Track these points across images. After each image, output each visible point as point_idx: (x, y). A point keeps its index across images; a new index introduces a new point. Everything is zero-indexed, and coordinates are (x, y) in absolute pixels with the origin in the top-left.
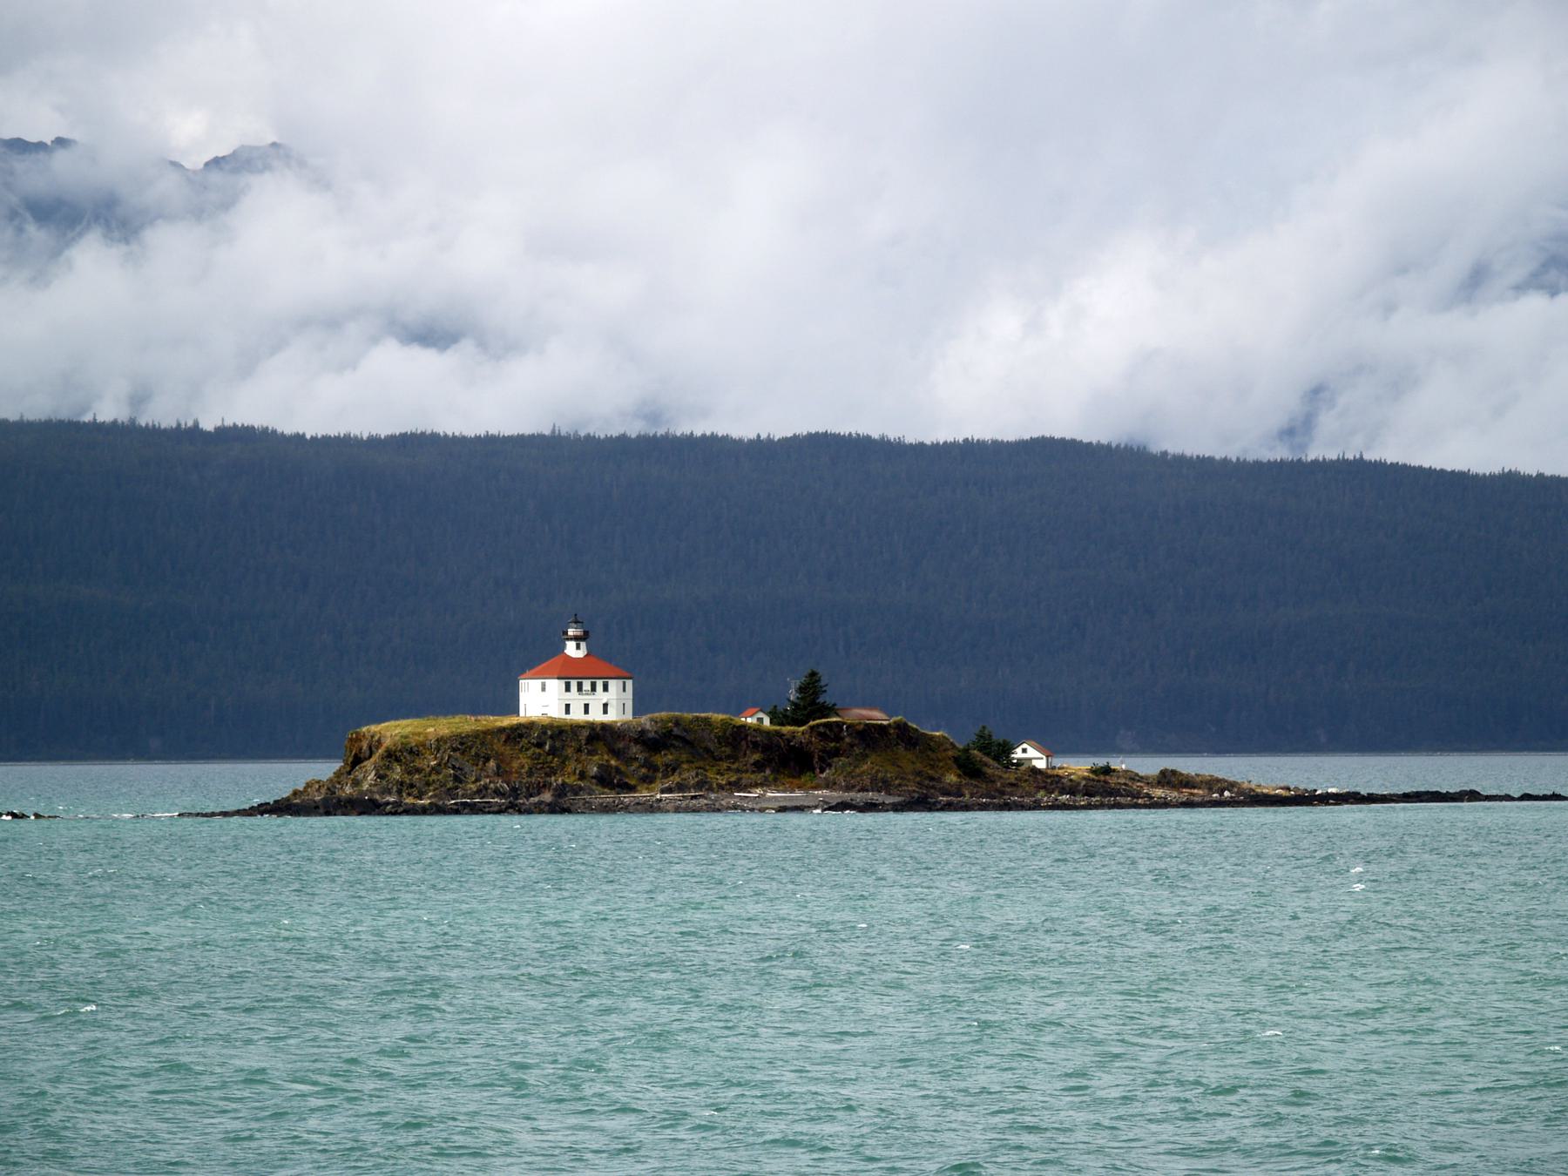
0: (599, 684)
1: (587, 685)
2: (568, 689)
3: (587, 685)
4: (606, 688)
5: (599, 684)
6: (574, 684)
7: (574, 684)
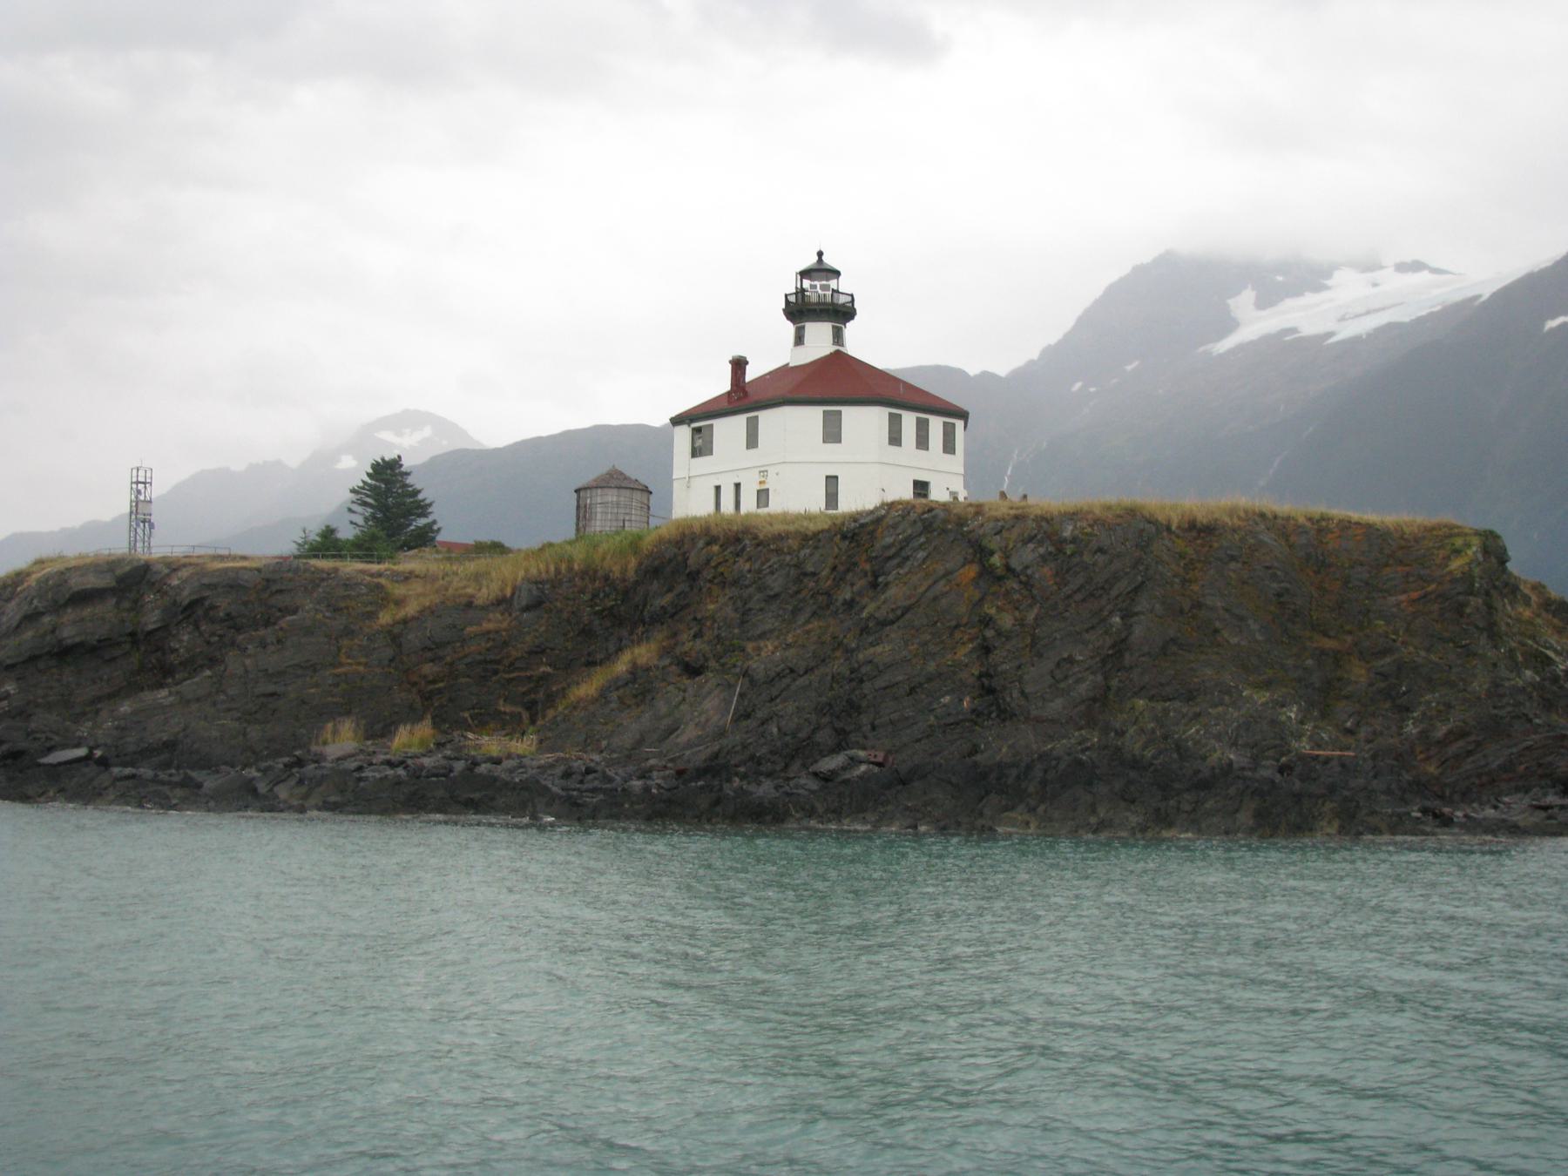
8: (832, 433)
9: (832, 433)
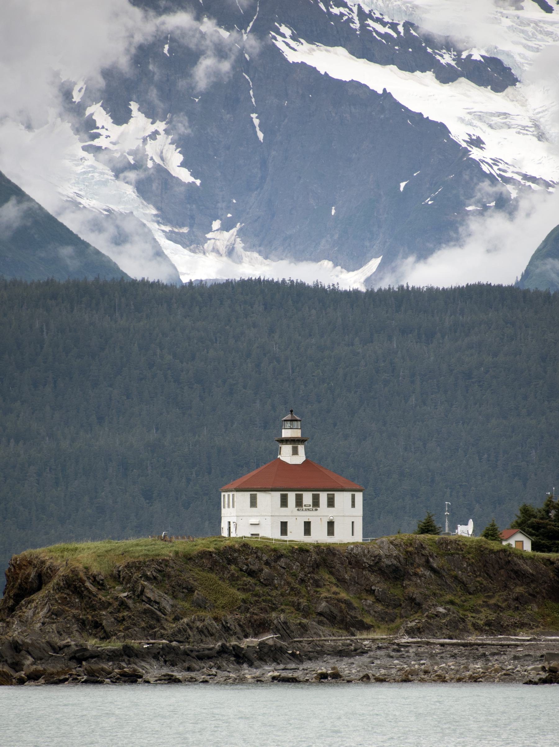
0: (323, 497)
1: (308, 498)
2: (284, 502)
3: (308, 498)
4: (331, 503)
5: (323, 497)
6: (292, 497)
7: (292, 497)
8: (253, 503)
9: (253, 503)
